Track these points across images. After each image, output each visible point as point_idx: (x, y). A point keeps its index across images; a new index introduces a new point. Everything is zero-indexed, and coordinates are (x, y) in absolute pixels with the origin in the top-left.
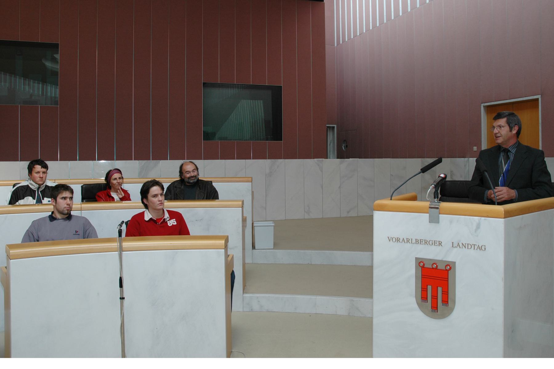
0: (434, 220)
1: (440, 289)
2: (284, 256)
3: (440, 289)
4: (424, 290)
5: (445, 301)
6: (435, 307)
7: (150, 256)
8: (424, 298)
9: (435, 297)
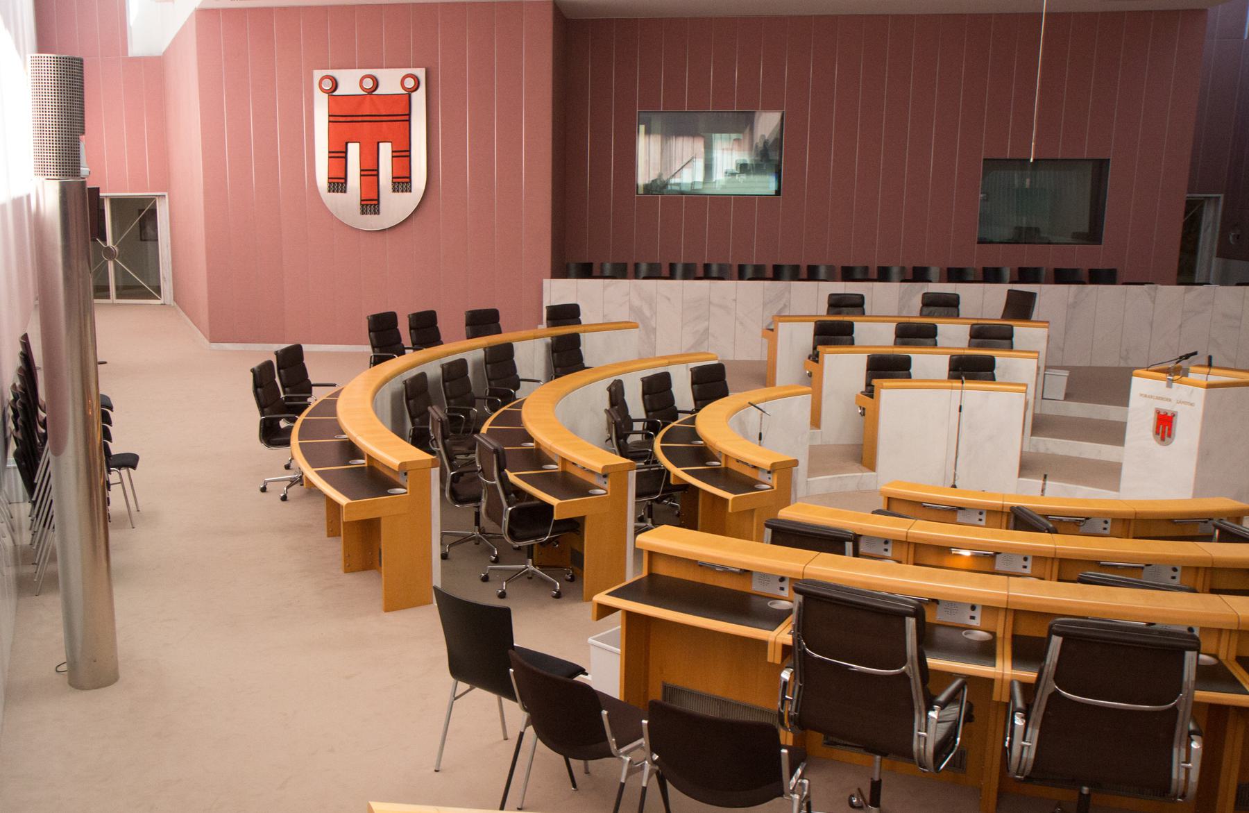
0: (1169, 386)
1: (386, 150)
2: (1078, 409)
3: (386, 150)
4: (1158, 428)
5: (1169, 435)
6: (1163, 439)
7: (974, 393)
8: (1157, 433)
9: (1164, 432)
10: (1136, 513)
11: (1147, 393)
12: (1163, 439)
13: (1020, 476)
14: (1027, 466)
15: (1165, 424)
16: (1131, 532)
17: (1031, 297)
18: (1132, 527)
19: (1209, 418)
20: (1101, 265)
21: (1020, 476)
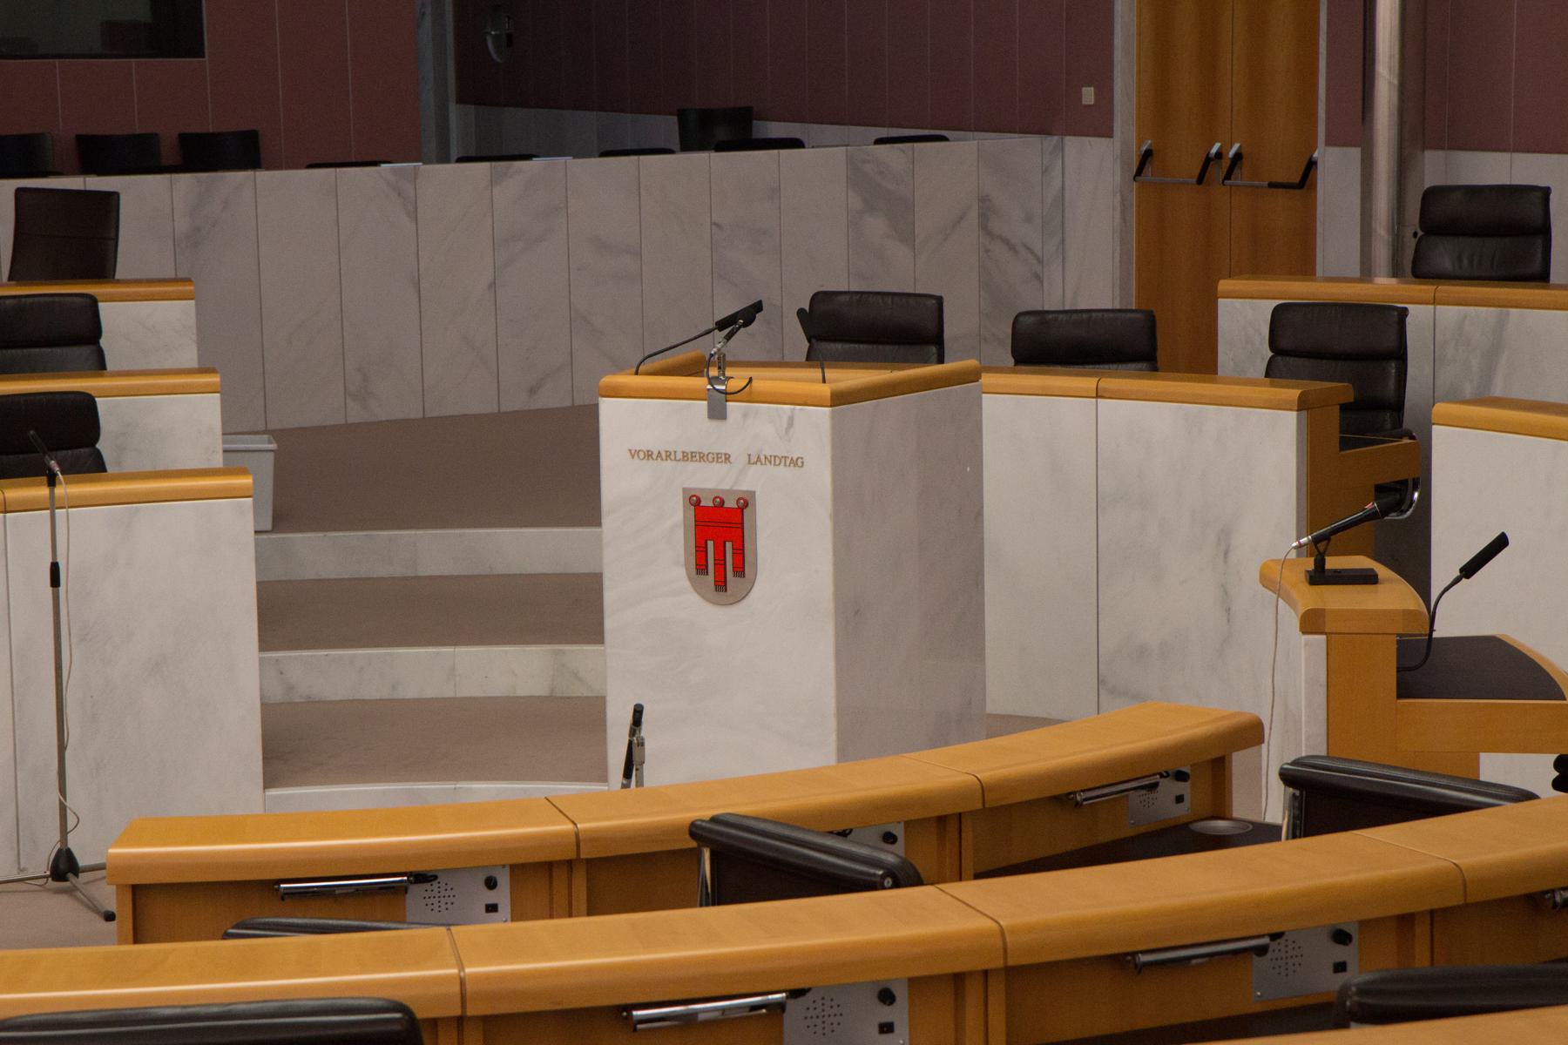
0: (718, 413)
4: (701, 551)
5: (740, 570)
6: (721, 584)
8: (701, 567)
10: (984, 789)
11: (649, 444)
12: (721, 584)
13: (269, 782)
14: (295, 745)
15: (720, 538)
16: (968, 866)
17: (109, 201)
18: (968, 835)
19: (851, 503)
20: (210, 123)
21: (269, 782)
